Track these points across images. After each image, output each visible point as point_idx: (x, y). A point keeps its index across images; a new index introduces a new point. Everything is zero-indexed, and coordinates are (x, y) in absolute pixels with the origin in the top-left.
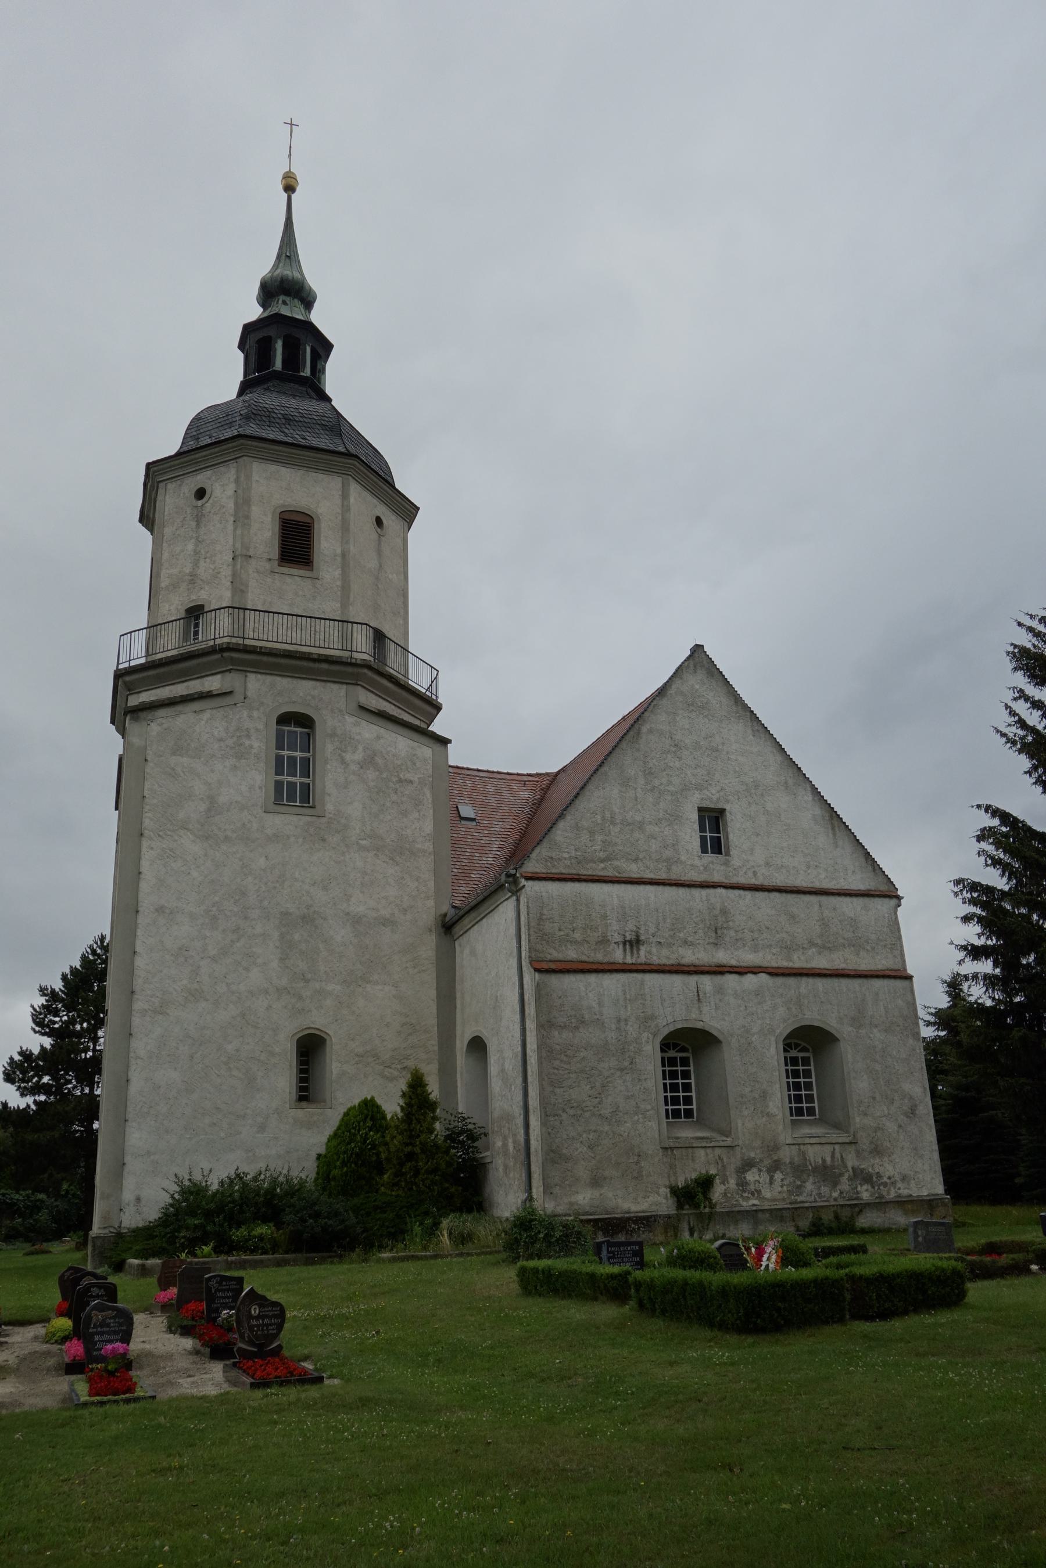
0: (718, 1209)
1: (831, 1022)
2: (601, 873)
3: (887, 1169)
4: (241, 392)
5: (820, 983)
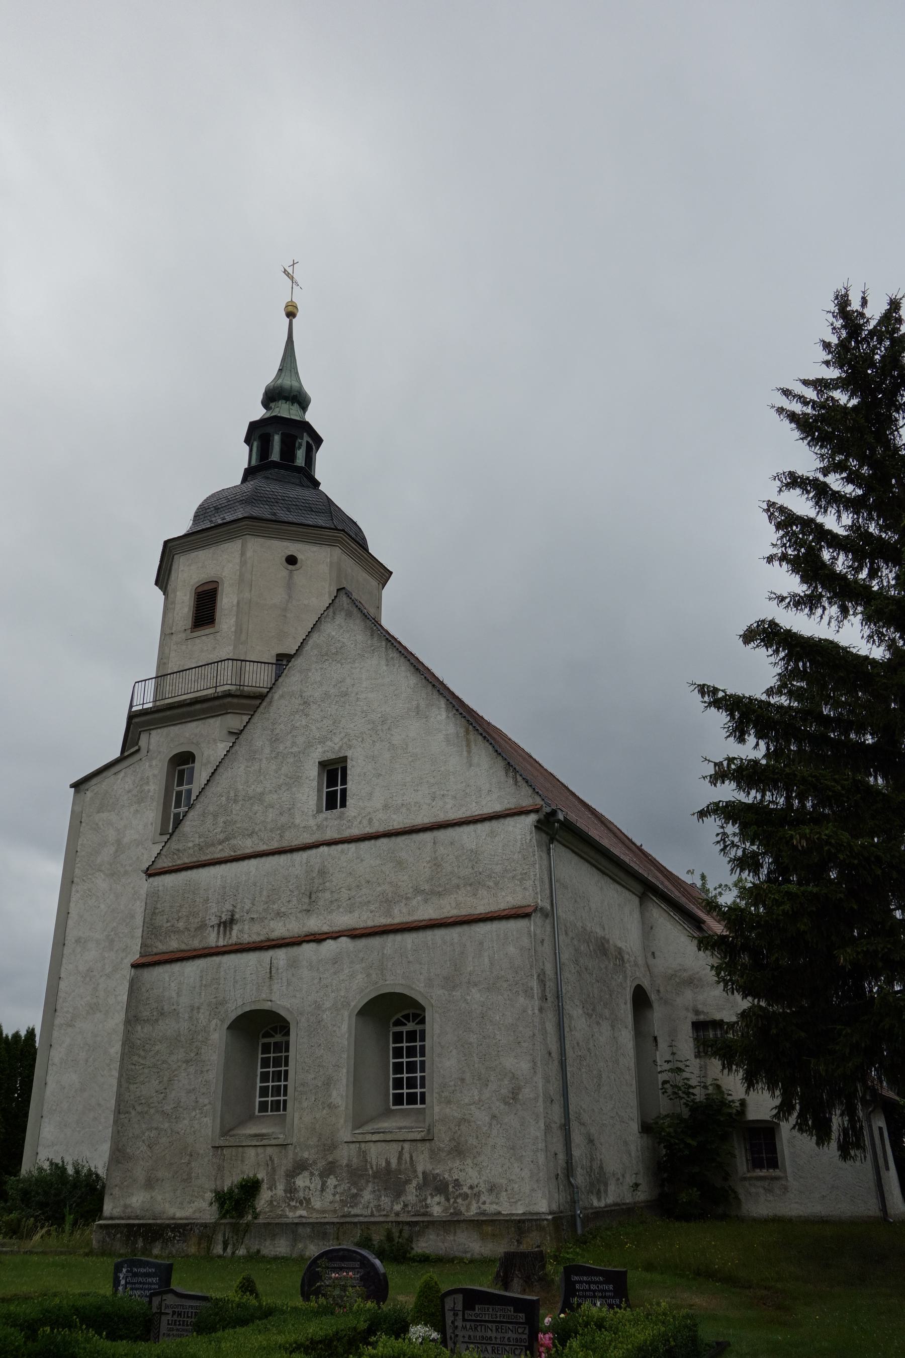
0: (261, 1220)
1: (418, 989)
2: (219, 856)
3: (469, 1175)
4: (245, 479)
5: (409, 940)
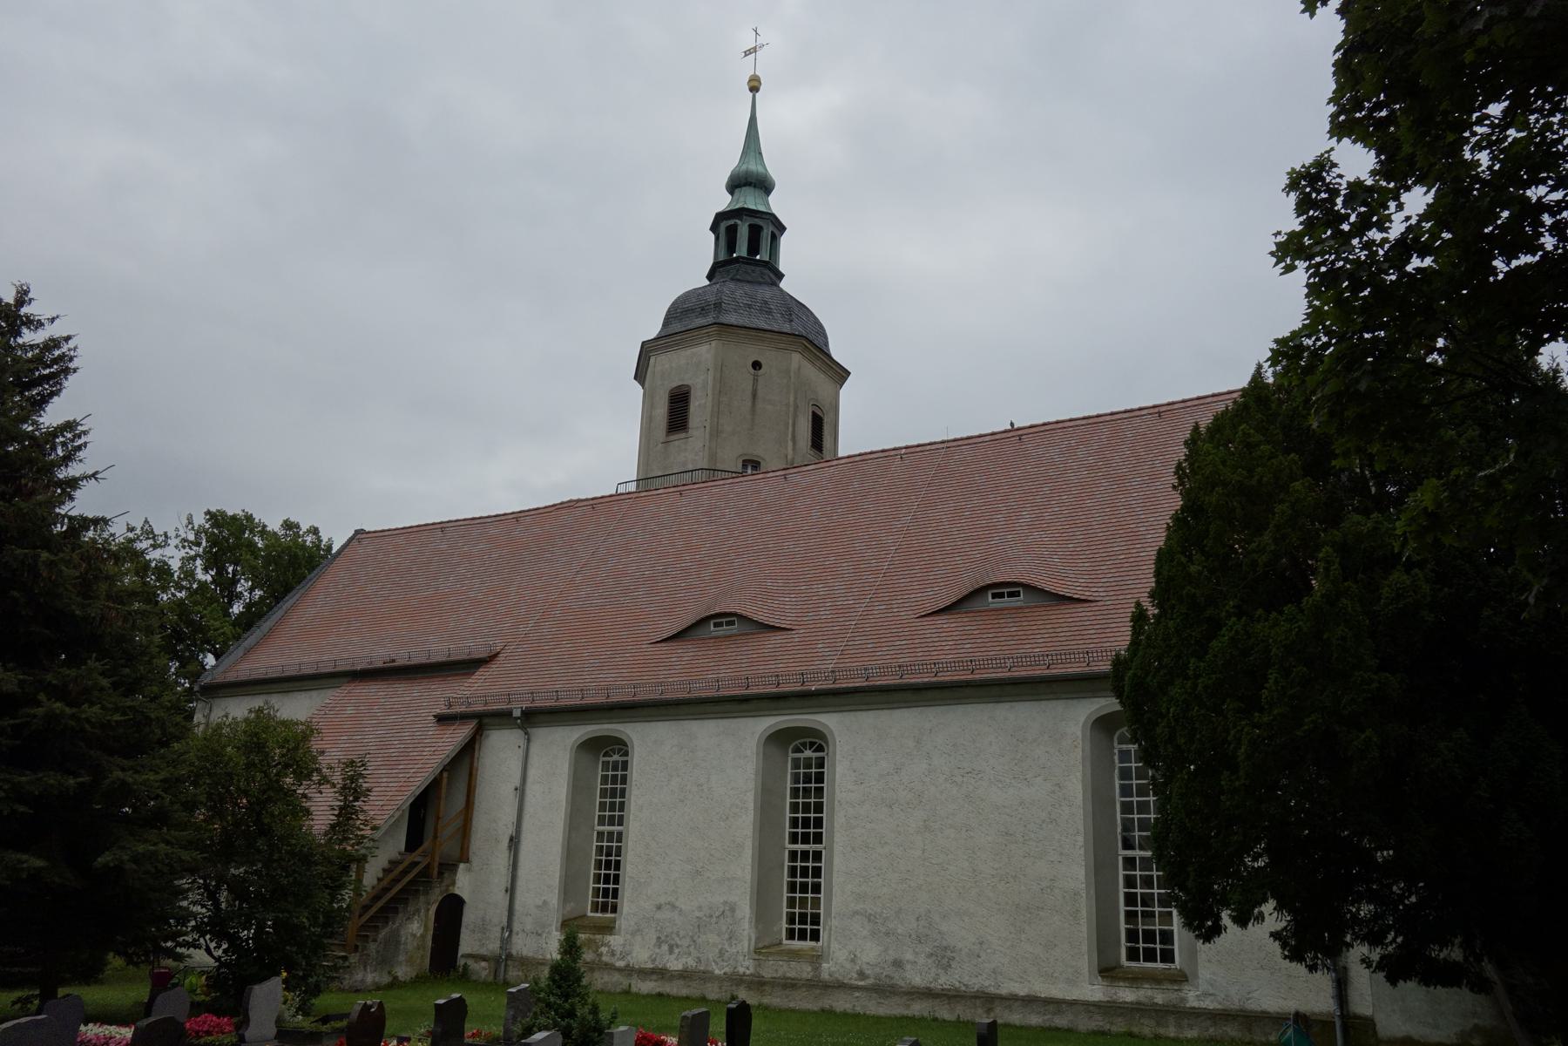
4: (710, 276)
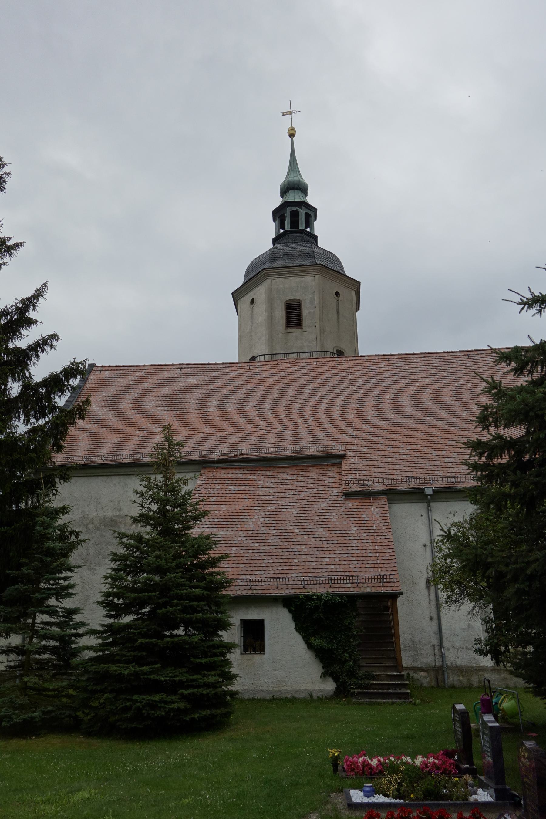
1: (297, 296)
4: (274, 245)
